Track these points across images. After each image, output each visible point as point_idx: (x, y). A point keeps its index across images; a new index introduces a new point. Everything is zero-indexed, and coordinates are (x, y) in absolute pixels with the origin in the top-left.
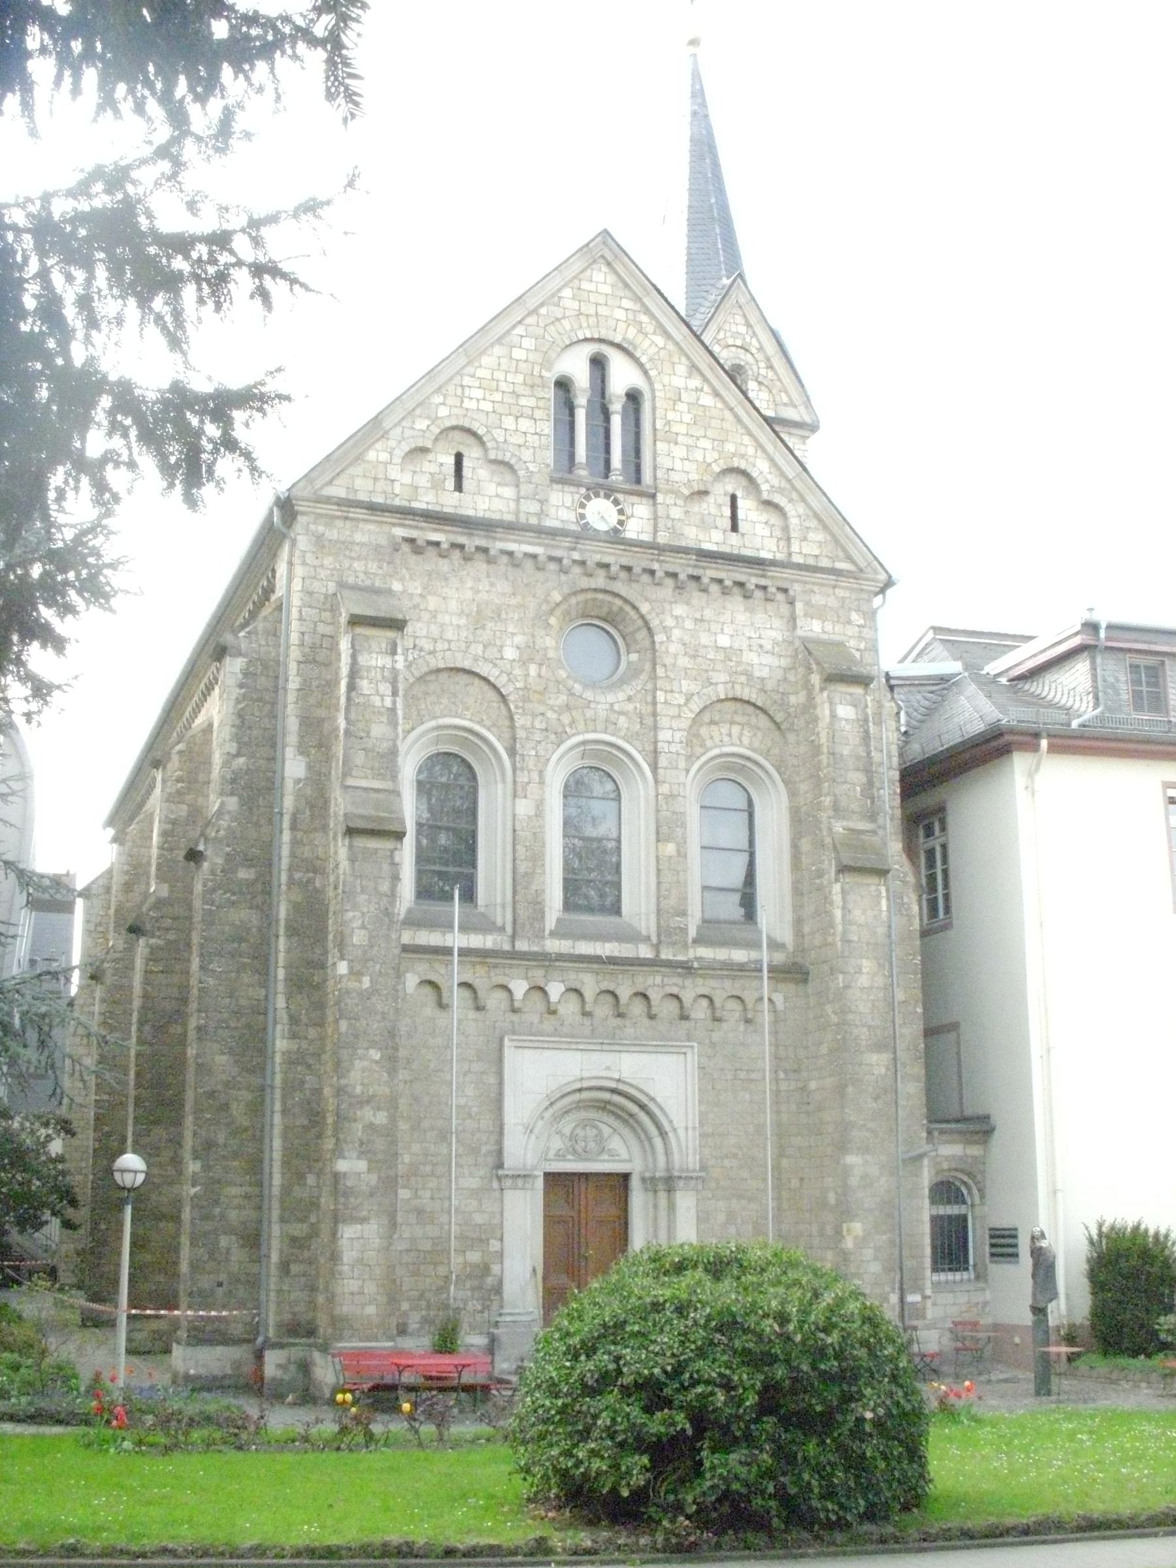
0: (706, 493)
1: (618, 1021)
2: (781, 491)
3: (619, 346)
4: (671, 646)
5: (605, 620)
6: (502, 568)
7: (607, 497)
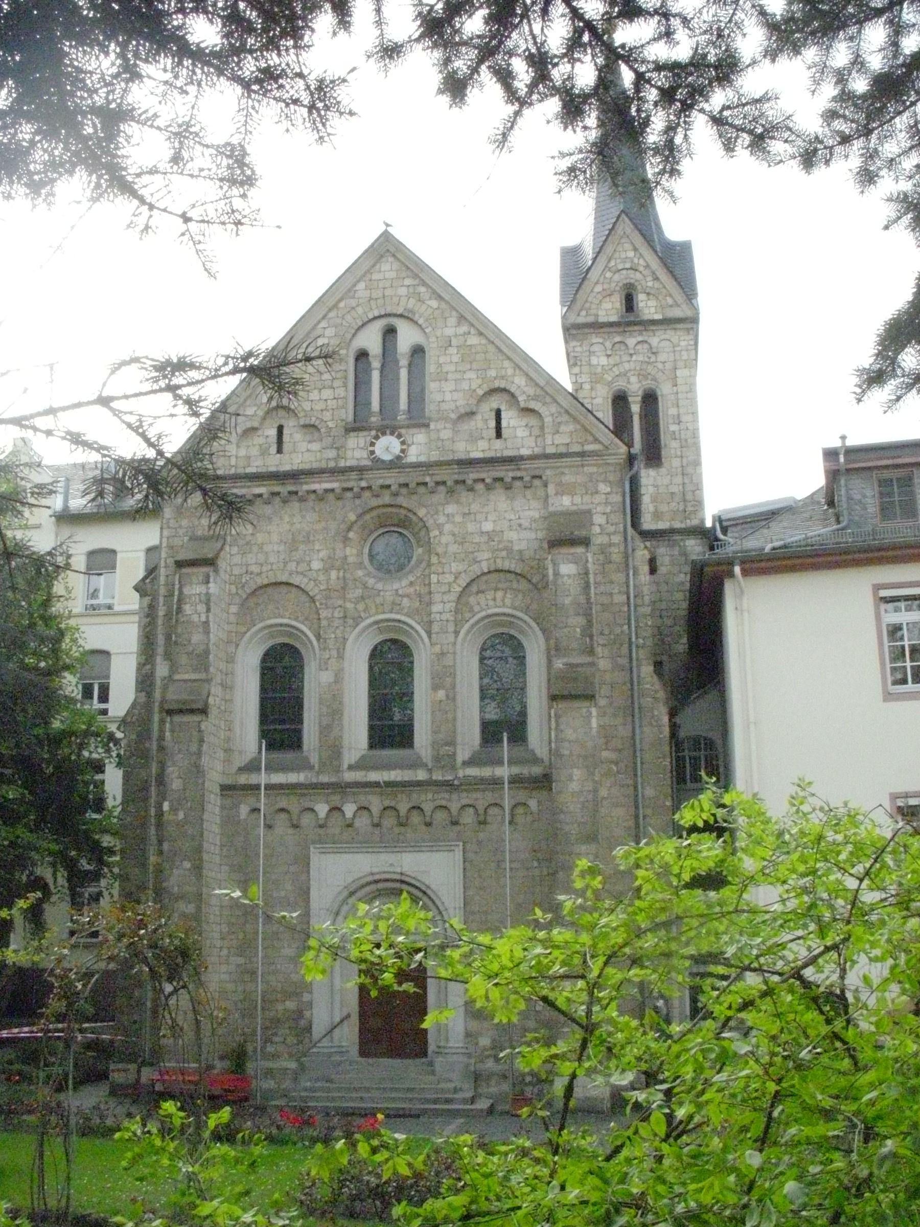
0: (473, 413)
1: (402, 829)
2: (536, 398)
5: (398, 526)
6: (311, 504)
7: (392, 434)
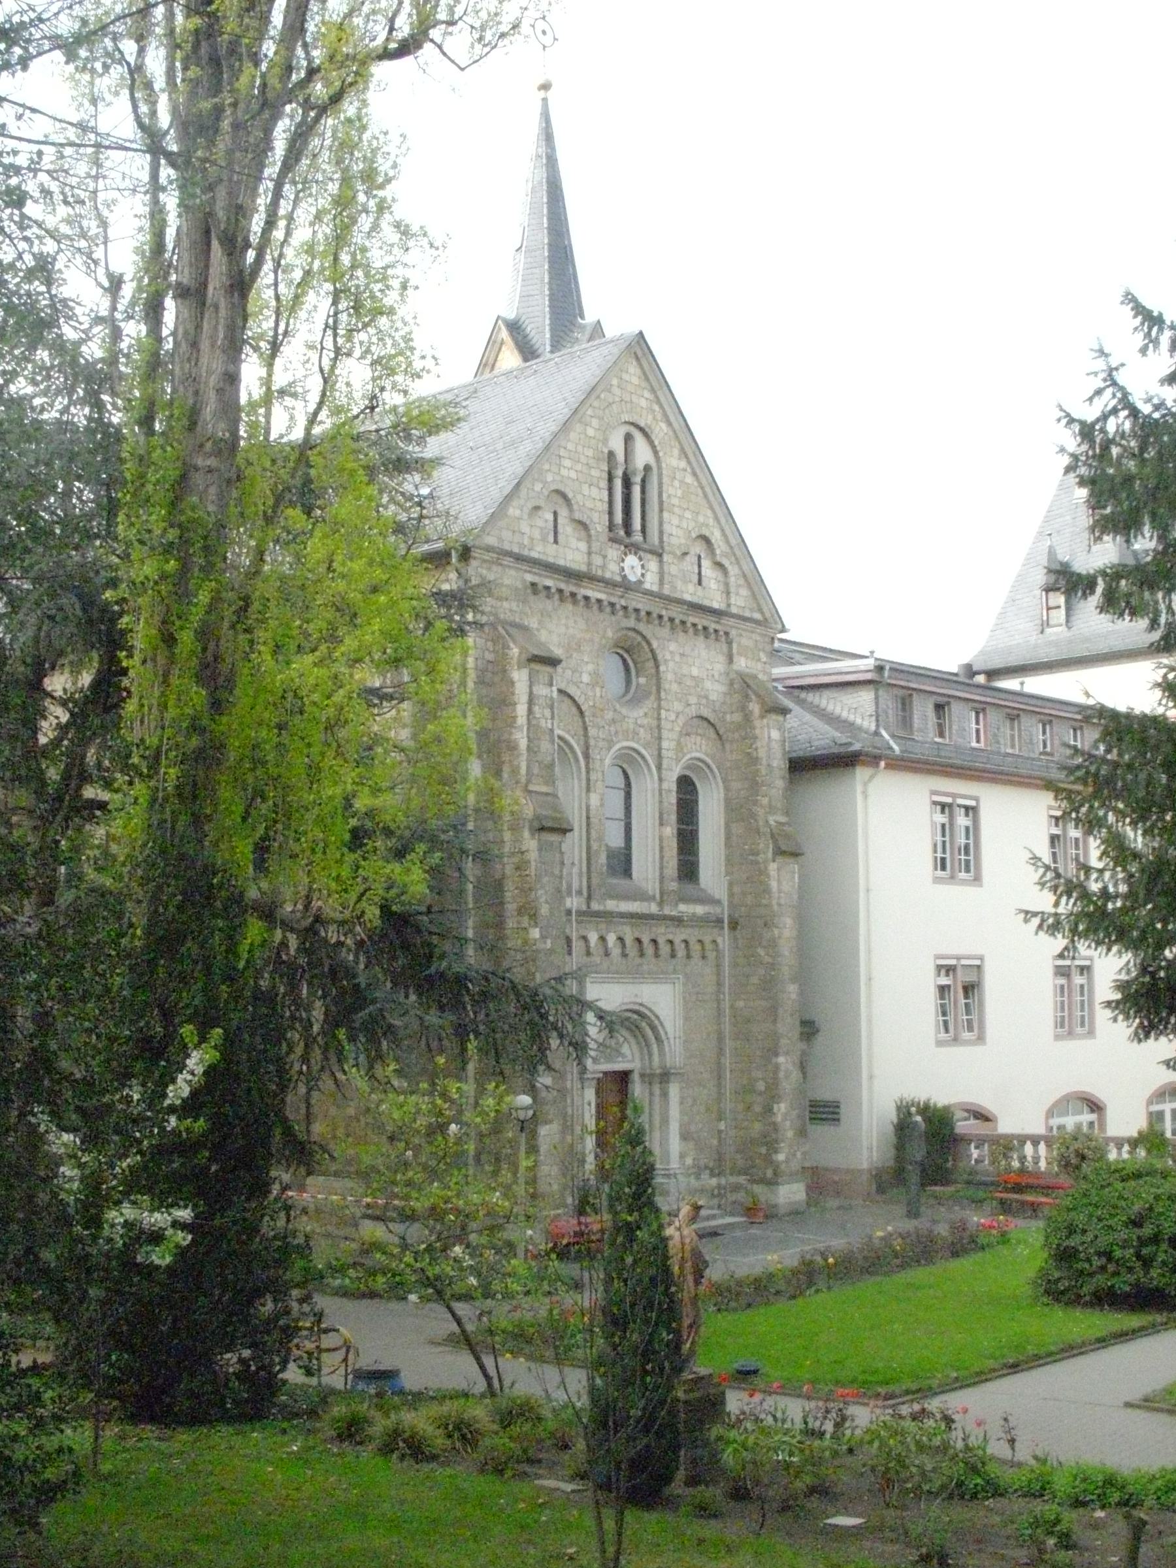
2: (725, 555)
3: (641, 429)
4: (668, 672)
